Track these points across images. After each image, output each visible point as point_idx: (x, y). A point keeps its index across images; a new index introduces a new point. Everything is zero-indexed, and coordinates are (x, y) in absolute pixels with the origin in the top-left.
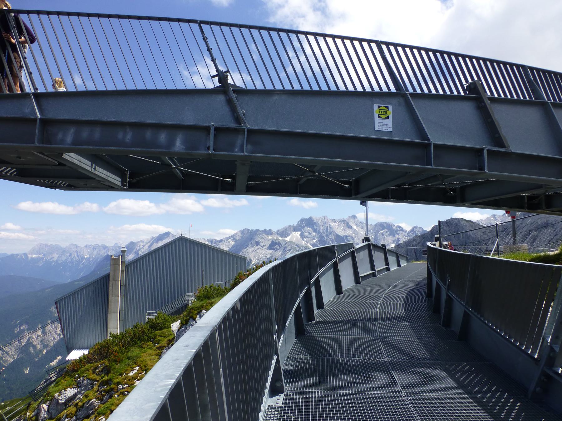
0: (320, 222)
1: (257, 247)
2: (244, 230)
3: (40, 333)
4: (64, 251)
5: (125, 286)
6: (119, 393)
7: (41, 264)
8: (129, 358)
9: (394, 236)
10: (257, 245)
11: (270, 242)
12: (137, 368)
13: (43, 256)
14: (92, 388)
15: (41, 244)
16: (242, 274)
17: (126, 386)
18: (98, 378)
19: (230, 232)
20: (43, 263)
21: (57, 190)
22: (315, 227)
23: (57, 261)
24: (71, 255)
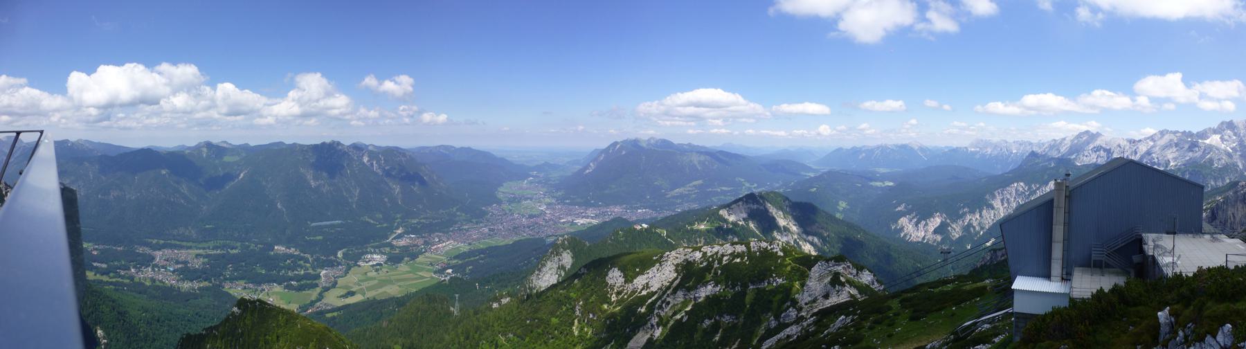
3: (978, 216)
4: (996, 146)
7: (978, 156)
16: (716, 265)
19: (1150, 131)
22: (1236, 131)
23: (991, 154)
24: (1001, 150)
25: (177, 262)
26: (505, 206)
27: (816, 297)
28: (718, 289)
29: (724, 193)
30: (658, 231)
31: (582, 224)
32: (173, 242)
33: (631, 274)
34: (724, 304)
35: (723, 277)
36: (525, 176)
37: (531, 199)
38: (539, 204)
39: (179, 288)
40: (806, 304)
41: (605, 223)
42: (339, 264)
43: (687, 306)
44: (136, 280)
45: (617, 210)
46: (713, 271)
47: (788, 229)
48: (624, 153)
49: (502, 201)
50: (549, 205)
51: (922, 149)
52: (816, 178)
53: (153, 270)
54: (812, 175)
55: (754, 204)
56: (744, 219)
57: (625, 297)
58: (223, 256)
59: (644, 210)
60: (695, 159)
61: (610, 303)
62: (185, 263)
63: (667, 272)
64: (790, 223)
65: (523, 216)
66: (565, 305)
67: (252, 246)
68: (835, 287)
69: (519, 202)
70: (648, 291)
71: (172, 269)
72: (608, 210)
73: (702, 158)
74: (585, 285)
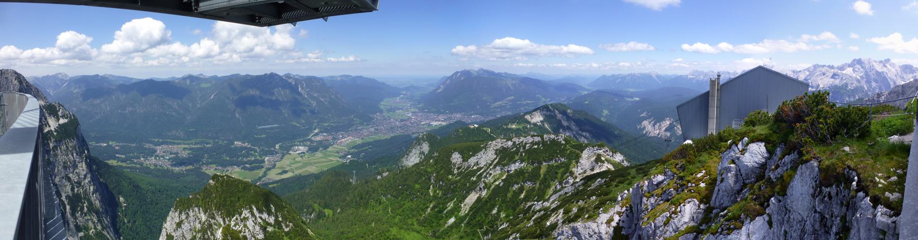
0: (866, 62)
1: (823, 77)
2: (815, 65)
5: (719, 100)
6: (688, 190)
7: (694, 81)
8: (699, 162)
9: (913, 74)
10: (824, 75)
11: (832, 74)
12: (704, 171)
14: (673, 178)
16: (522, 150)
17: (694, 185)
18: (678, 172)
23: (703, 80)
25: (171, 153)
26: (385, 114)
28: (522, 165)
29: (528, 105)
32: (168, 140)
35: (526, 158)
36: (398, 94)
37: (402, 109)
39: (172, 170)
40: (579, 174)
42: (277, 153)
43: (503, 176)
44: (145, 165)
45: (458, 116)
46: (519, 154)
48: (462, 78)
50: (413, 113)
51: (658, 76)
53: (155, 158)
54: (586, 93)
56: (541, 121)
58: (201, 149)
60: (509, 83)
61: (453, 175)
62: (177, 153)
63: (490, 154)
67: (220, 142)
68: (598, 164)
69: (394, 111)
71: (168, 158)
73: (514, 82)
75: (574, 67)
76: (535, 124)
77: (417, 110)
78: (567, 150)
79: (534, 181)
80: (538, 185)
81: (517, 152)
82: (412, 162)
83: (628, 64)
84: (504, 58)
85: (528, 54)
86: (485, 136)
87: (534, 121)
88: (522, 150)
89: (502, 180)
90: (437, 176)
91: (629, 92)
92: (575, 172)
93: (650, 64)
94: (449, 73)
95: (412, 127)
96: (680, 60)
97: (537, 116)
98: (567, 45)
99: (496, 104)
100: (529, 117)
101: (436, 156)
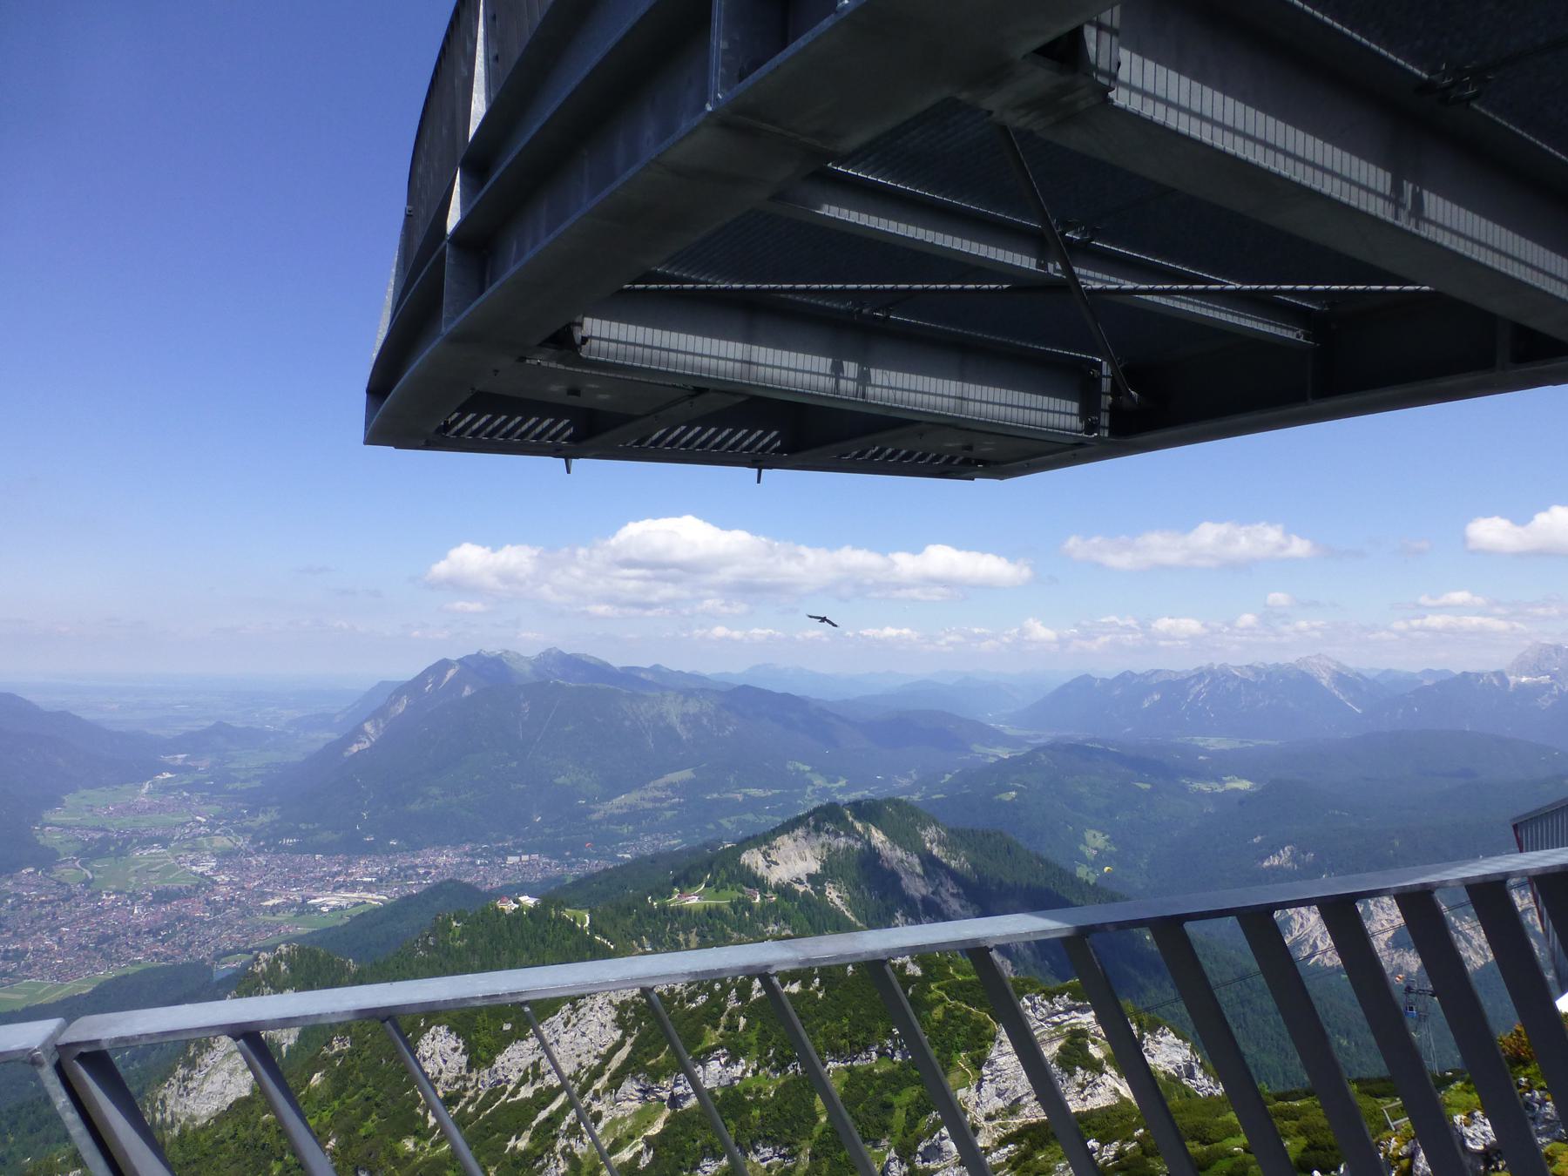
7: (1545, 702)
13: (1551, 679)
15: (1544, 644)
16: (732, 1004)
20: (1550, 702)
21: (581, 459)
26: (70, 872)
27: (1019, 1099)
28: (737, 1071)
29: (752, 804)
30: (568, 914)
31: (333, 910)
33: (486, 1040)
34: (756, 1113)
35: (753, 1037)
36: (145, 770)
37: (164, 842)
38: (191, 857)
40: (989, 1118)
41: (408, 900)
43: (650, 1123)
45: (444, 861)
46: (723, 1020)
47: (938, 906)
48: (467, 691)
49: (57, 855)
50: (225, 856)
51: (1345, 680)
52: (1014, 762)
54: (1004, 753)
55: (837, 835)
56: (810, 877)
57: (470, 1109)
59: (525, 858)
60: (673, 711)
61: (422, 1134)
63: (595, 1027)
64: (943, 890)
65: (135, 897)
66: (281, 1159)
68: (1072, 1074)
69: (121, 852)
70: (537, 1086)
72: (418, 861)
73: (692, 707)
74: (343, 1089)
75: (950, 644)
76: (785, 891)
77: (242, 843)
78: (930, 1006)
79: (788, 1145)
80: (804, 1158)
81: (711, 1014)
82: (210, 1096)
83: (1192, 625)
84: (648, 606)
85: (749, 590)
86: (568, 943)
87: (778, 875)
88: (732, 1004)
89: (649, 1142)
90: (344, 1147)
91: (1203, 751)
92: (970, 1106)
93: (1303, 624)
94: (407, 669)
95: (214, 923)
96: (1460, 597)
97: (794, 855)
98: (917, 549)
99: (616, 801)
100: (760, 857)
101: (339, 1055)
